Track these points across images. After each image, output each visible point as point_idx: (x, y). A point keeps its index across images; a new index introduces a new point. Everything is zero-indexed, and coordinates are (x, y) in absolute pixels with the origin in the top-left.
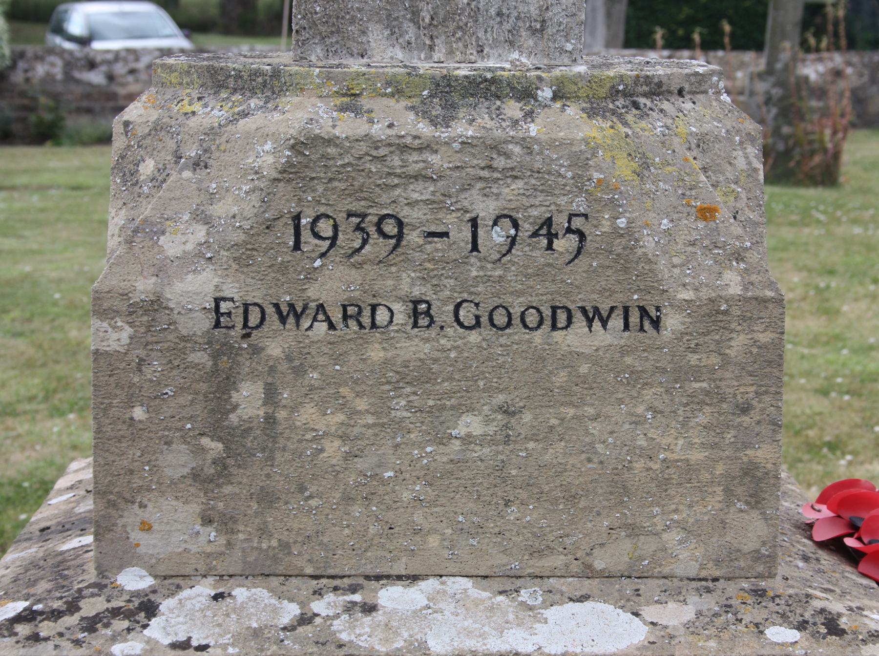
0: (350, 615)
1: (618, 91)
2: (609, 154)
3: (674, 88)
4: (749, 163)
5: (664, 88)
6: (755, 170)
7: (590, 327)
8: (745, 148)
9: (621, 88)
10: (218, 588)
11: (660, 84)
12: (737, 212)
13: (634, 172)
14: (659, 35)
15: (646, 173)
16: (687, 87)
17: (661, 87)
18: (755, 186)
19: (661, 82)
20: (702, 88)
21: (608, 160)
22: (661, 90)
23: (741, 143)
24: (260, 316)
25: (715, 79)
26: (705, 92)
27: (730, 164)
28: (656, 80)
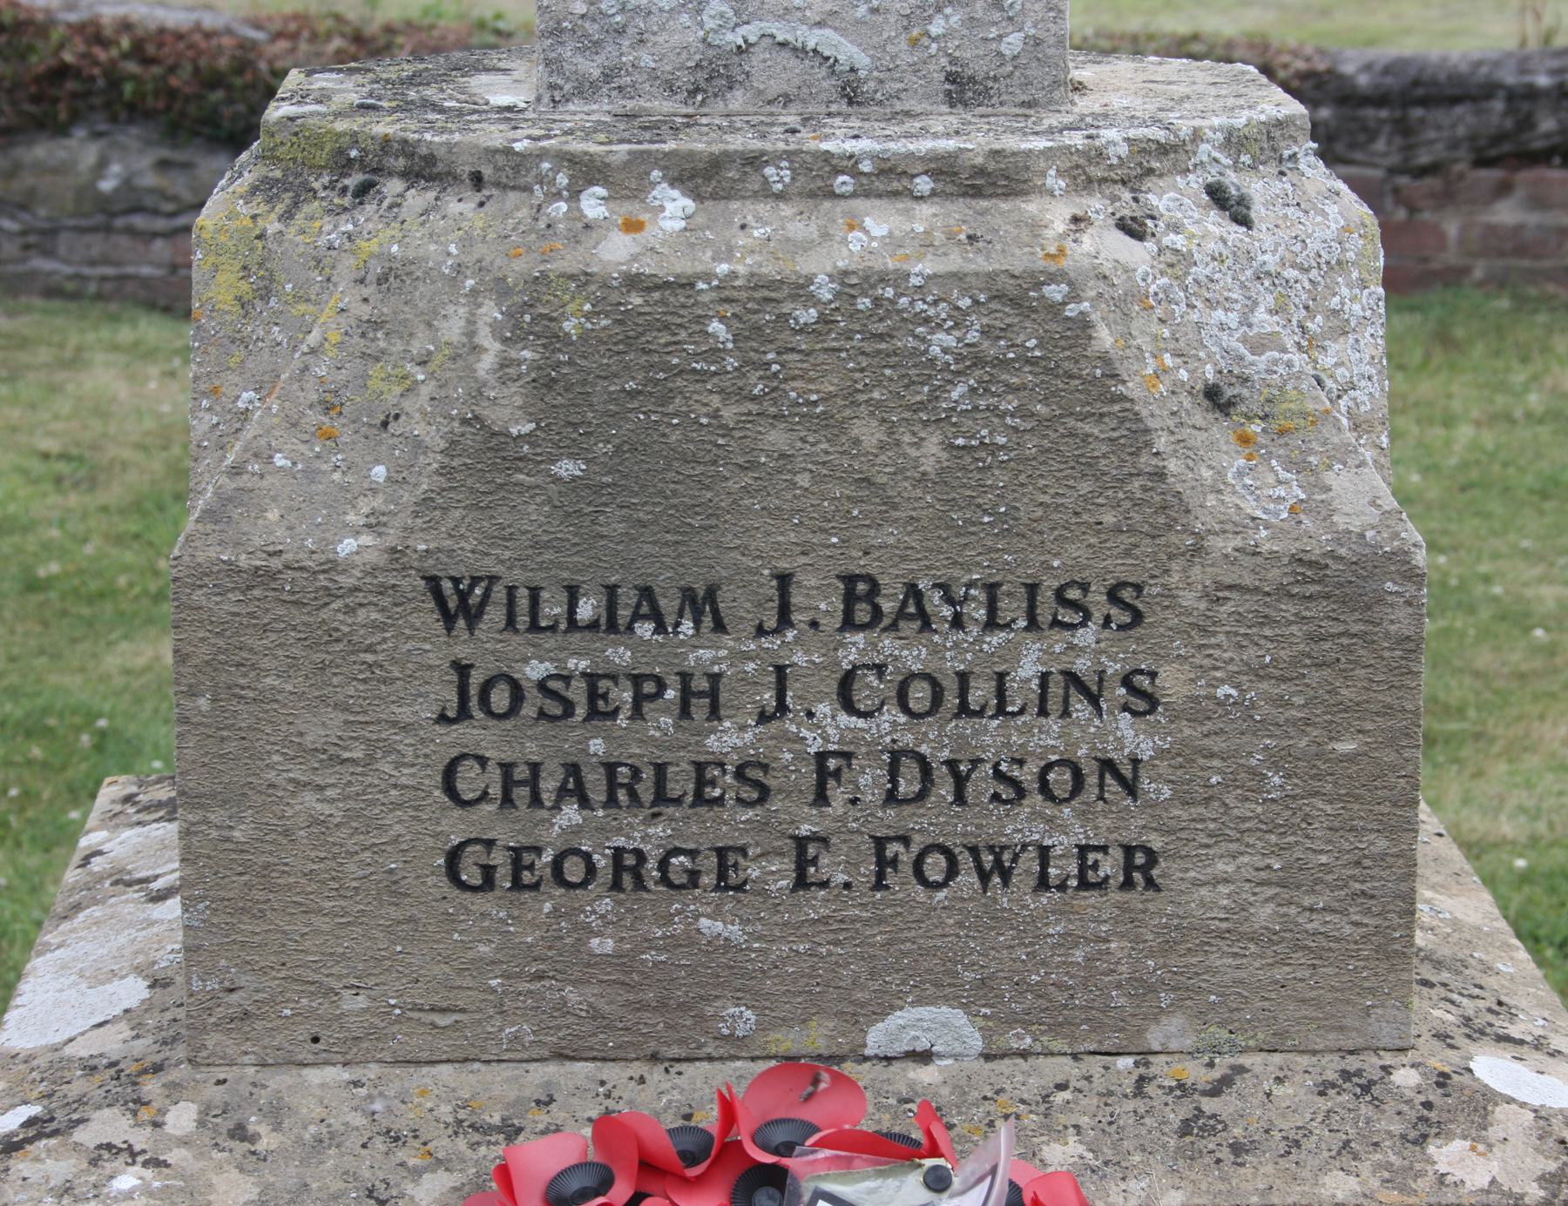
0: (338, 1146)
1: (350, 161)
2: (212, 259)
3: (465, 170)
4: (471, 334)
5: (440, 167)
6: (476, 349)
7: (449, 629)
8: (479, 306)
9: (354, 153)
10: (774, 1166)
11: (430, 160)
12: (397, 417)
13: (238, 298)
14: (1325, 113)
15: (259, 305)
16: (487, 171)
17: (434, 165)
18: (460, 378)
19: (432, 155)
20: (522, 181)
21: (206, 268)
22: (435, 170)
23: (474, 292)
24: (1039, 611)
25: (546, 165)
26: (527, 189)
27: (430, 325)
28: (423, 151)
